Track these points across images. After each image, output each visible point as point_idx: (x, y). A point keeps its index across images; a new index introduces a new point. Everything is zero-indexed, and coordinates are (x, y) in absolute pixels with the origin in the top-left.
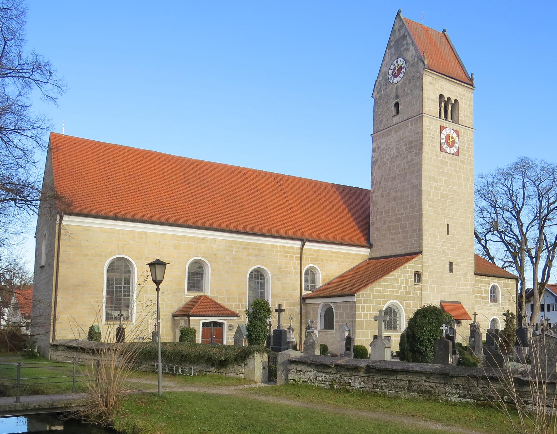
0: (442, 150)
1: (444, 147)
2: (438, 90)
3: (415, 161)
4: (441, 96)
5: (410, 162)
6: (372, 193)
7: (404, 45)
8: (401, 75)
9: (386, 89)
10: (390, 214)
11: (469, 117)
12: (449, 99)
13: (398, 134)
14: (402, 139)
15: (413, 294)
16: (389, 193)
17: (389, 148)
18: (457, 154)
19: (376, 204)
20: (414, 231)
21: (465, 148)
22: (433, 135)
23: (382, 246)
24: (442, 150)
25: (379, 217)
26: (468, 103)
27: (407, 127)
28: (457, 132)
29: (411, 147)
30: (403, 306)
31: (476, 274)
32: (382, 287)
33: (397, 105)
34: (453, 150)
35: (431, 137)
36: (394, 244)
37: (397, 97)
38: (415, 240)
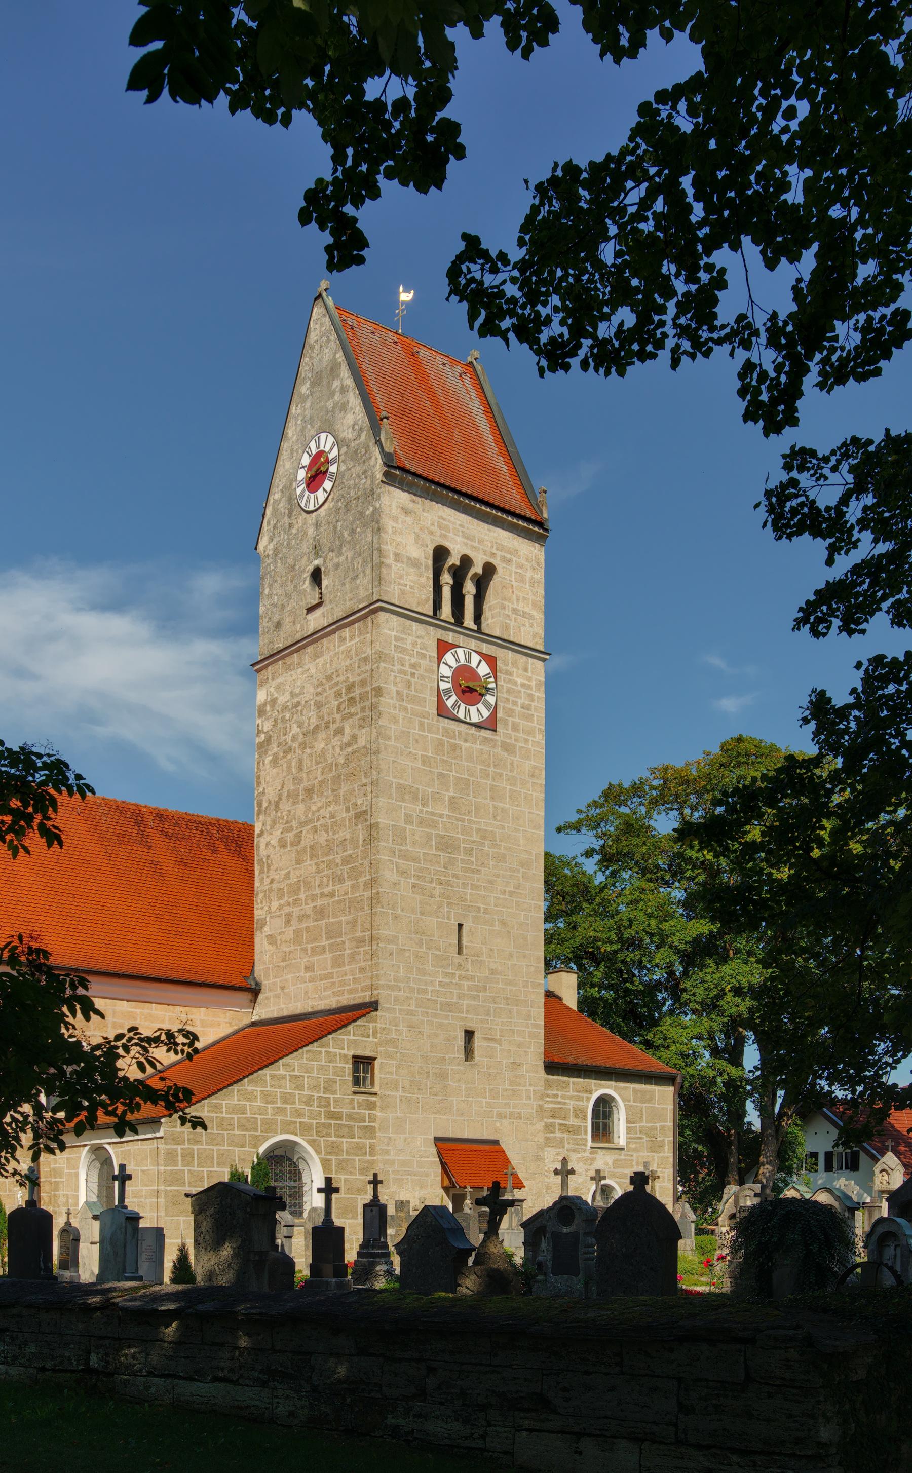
0: (443, 712)
1: (449, 703)
2: (431, 533)
3: (362, 742)
4: (440, 554)
5: (349, 744)
6: (260, 835)
7: (332, 394)
8: (328, 485)
9: (291, 526)
10: (302, 896)
11: (531, 617)
12: (466, 561)
13: (321, 661)
14: (329, 678)
15: (350, 1117)
16: (299, 835)
17: (298, 704)
18: (490, 725)
19: (269, 866)
20: (360, 942)
21: (518, 709)
22: (413, 666)
23: (282, 988)
24: (443, 712)
25: (275, 905)
26: (529, 575)
27: (342, 640)
28: (491, 661)
29: (352, 701)
30: (318, 1152)
31: (552, 1067)
32: (249, 1100)
33: (316, 576)
34: (478, 713)
35: (405, 673)
36: (312, 980)
37: (317, 550)
38: (362, 970)
